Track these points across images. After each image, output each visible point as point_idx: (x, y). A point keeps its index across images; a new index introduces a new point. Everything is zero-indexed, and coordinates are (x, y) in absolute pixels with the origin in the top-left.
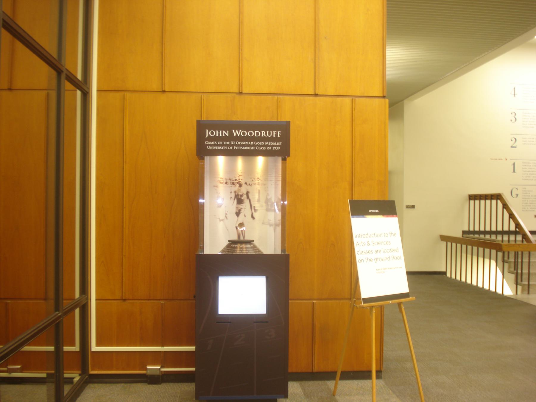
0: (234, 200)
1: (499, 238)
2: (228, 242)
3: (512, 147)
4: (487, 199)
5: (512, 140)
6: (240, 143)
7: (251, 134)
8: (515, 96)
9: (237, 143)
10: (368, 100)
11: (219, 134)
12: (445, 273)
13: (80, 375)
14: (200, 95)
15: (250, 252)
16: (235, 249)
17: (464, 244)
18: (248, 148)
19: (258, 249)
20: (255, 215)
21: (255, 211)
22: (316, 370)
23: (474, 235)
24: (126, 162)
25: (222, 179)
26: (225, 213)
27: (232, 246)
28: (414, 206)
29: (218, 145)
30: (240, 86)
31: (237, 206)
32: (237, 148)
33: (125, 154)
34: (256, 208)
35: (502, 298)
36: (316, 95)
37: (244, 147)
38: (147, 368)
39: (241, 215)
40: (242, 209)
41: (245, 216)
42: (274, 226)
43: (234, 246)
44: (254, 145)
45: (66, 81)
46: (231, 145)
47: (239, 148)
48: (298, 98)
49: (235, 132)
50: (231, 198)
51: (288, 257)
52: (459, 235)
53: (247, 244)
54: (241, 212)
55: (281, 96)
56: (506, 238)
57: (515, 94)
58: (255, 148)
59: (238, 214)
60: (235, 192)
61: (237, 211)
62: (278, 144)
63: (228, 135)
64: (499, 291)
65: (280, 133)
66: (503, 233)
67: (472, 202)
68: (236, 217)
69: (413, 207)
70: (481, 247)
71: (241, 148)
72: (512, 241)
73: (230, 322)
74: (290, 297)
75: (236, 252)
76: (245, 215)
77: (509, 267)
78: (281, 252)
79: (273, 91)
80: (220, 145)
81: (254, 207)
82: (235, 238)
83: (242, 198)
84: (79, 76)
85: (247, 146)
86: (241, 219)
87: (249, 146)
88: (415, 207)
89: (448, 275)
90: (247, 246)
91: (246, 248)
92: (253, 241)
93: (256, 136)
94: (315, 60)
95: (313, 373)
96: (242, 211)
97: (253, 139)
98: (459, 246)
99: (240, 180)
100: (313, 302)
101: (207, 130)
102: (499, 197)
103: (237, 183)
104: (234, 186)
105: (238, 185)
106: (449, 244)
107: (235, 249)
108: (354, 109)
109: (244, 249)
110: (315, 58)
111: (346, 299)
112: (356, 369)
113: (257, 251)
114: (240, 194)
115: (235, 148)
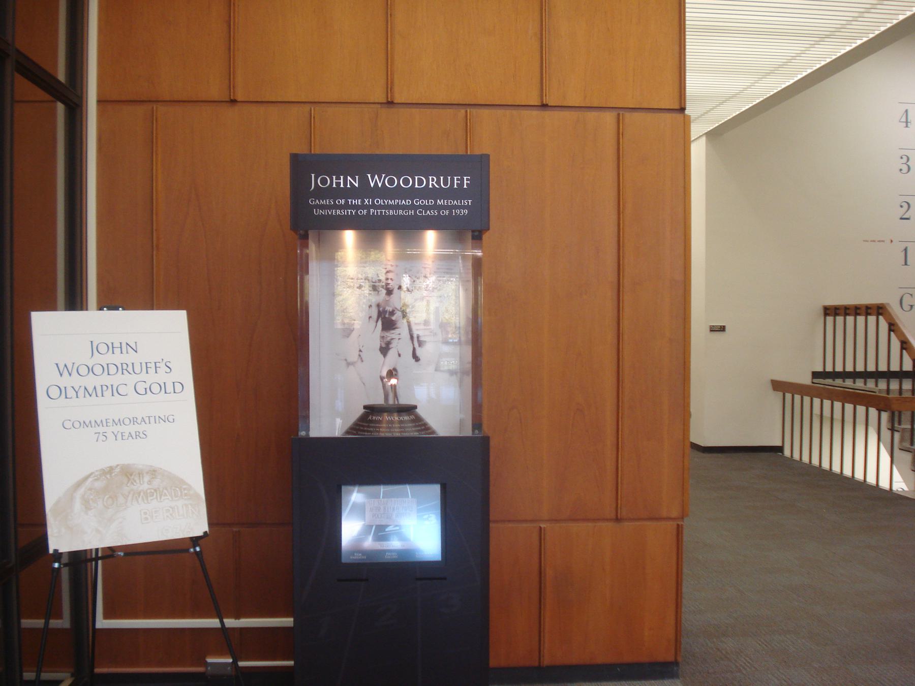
0: (377, 321)
1: (882, 385)
2: (361, 411)
3: (901, 219)
4: (849, 314)
5: (901, 206)
6: (384, 202)
7: (406, 182)
8: (907, 126)
9: (378, 202)
10: (649, 116)
11: (338, 184)
12: (780, 449)
13: (72, 675)
14: (306, 108)
15: (408, 432)
16: (377, 425)
17: (807, 395)
18: (401, 212)
19: (425, 424)
20: (419, 352)
21: (421, 344)
22: (546, 661)
23: (834, 380)
24: (157, 246)
25: (352, 279)
26: (358, 350)
27: (370, 418)
28: (724, 326)
29: (336, 207)
30: (389, 89)
31: (382, 335)
32: (377, 212)
33: (156, 230)
34: (421, 339)
35: (890, 497)
36: (544, 106)
37: (391, 211)
38: (206, 661)
39: (392, 353)
40: (392, 341)
41: (399, 355)
42: (459, 375)
43: (374, 418)
44: (413, 207)
45: (17, 75)
46: (363, 207)
47: (382, 212)
48: (508, 112)
49: (373, 178)
50: (370, 317)
51: (486, 440)
52: (807, 380)
53: (402, 413)
54: (391, 346)
55: (471, 110)
56: (894, 385)
57: (907, 122)
58: (415, 212)
59: (385, 350)
60: (378, 306)
61: (384, 346)
62: (464, 203)
63: (357, 185)
64: (884, 484)
65: (467, 180)
66: (889, 375)
67: (830, 319)
68: (382, 356)
69: (722, 329)
70: (828, 399)
71: (385, 212)
72: (907, 390)
73: (367, 580)
74: (492, 518)
75: (379, 432)
76: (400, 352)
77: (902, 440)
78: (473, 431)
79: (456, 98)
80: (340, 207)
81: (418, 337)
82: (379, 400)
83: (394, 318)
84: (61, 76)
85: (397, 207)
86: (391, 360)
87: (404, 207)
88: (727, 329)
89: (787, 452)
90: (401, 418)
91: (401, 422)
92: (415, 407)
93: (416, 186)
94: (542, 35)
95: (539, 668)
96: (394, 345)
97: (412, 193)
98: (797, 398)
99: (389, 281)
100: (540, 527)
101: (313, 175)
102: (880, 311)
103: (382, 287)
104: (377, 292)
105: (384, 292)
106: (788, 396)
107: (377, 425)
108: (622, 135)
109: (397, 425)
110: (542, 30)
111: (607, 520)
112: (627, 659)
113: (423, 428)
114: (389, 309)
115: (373, 213)
